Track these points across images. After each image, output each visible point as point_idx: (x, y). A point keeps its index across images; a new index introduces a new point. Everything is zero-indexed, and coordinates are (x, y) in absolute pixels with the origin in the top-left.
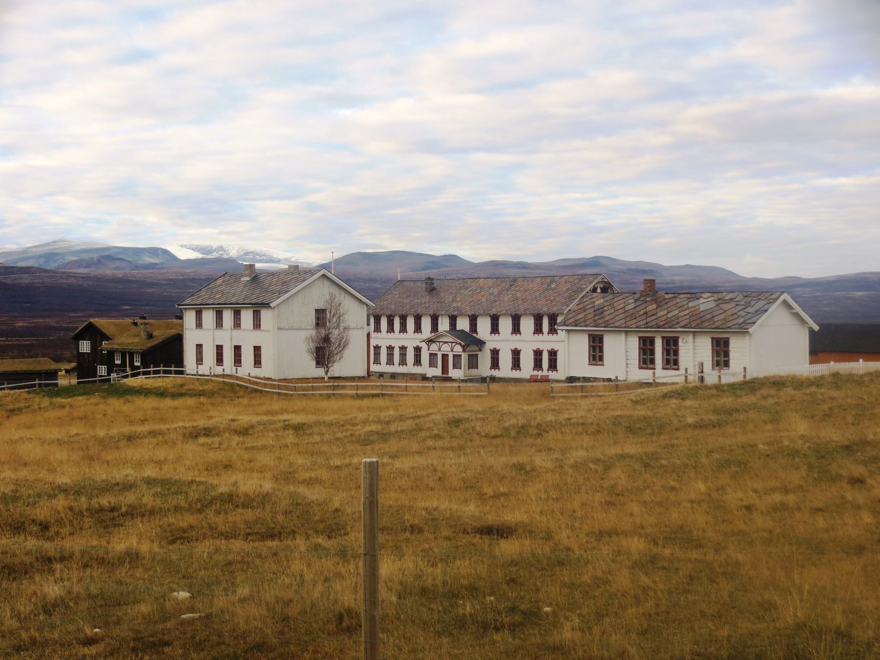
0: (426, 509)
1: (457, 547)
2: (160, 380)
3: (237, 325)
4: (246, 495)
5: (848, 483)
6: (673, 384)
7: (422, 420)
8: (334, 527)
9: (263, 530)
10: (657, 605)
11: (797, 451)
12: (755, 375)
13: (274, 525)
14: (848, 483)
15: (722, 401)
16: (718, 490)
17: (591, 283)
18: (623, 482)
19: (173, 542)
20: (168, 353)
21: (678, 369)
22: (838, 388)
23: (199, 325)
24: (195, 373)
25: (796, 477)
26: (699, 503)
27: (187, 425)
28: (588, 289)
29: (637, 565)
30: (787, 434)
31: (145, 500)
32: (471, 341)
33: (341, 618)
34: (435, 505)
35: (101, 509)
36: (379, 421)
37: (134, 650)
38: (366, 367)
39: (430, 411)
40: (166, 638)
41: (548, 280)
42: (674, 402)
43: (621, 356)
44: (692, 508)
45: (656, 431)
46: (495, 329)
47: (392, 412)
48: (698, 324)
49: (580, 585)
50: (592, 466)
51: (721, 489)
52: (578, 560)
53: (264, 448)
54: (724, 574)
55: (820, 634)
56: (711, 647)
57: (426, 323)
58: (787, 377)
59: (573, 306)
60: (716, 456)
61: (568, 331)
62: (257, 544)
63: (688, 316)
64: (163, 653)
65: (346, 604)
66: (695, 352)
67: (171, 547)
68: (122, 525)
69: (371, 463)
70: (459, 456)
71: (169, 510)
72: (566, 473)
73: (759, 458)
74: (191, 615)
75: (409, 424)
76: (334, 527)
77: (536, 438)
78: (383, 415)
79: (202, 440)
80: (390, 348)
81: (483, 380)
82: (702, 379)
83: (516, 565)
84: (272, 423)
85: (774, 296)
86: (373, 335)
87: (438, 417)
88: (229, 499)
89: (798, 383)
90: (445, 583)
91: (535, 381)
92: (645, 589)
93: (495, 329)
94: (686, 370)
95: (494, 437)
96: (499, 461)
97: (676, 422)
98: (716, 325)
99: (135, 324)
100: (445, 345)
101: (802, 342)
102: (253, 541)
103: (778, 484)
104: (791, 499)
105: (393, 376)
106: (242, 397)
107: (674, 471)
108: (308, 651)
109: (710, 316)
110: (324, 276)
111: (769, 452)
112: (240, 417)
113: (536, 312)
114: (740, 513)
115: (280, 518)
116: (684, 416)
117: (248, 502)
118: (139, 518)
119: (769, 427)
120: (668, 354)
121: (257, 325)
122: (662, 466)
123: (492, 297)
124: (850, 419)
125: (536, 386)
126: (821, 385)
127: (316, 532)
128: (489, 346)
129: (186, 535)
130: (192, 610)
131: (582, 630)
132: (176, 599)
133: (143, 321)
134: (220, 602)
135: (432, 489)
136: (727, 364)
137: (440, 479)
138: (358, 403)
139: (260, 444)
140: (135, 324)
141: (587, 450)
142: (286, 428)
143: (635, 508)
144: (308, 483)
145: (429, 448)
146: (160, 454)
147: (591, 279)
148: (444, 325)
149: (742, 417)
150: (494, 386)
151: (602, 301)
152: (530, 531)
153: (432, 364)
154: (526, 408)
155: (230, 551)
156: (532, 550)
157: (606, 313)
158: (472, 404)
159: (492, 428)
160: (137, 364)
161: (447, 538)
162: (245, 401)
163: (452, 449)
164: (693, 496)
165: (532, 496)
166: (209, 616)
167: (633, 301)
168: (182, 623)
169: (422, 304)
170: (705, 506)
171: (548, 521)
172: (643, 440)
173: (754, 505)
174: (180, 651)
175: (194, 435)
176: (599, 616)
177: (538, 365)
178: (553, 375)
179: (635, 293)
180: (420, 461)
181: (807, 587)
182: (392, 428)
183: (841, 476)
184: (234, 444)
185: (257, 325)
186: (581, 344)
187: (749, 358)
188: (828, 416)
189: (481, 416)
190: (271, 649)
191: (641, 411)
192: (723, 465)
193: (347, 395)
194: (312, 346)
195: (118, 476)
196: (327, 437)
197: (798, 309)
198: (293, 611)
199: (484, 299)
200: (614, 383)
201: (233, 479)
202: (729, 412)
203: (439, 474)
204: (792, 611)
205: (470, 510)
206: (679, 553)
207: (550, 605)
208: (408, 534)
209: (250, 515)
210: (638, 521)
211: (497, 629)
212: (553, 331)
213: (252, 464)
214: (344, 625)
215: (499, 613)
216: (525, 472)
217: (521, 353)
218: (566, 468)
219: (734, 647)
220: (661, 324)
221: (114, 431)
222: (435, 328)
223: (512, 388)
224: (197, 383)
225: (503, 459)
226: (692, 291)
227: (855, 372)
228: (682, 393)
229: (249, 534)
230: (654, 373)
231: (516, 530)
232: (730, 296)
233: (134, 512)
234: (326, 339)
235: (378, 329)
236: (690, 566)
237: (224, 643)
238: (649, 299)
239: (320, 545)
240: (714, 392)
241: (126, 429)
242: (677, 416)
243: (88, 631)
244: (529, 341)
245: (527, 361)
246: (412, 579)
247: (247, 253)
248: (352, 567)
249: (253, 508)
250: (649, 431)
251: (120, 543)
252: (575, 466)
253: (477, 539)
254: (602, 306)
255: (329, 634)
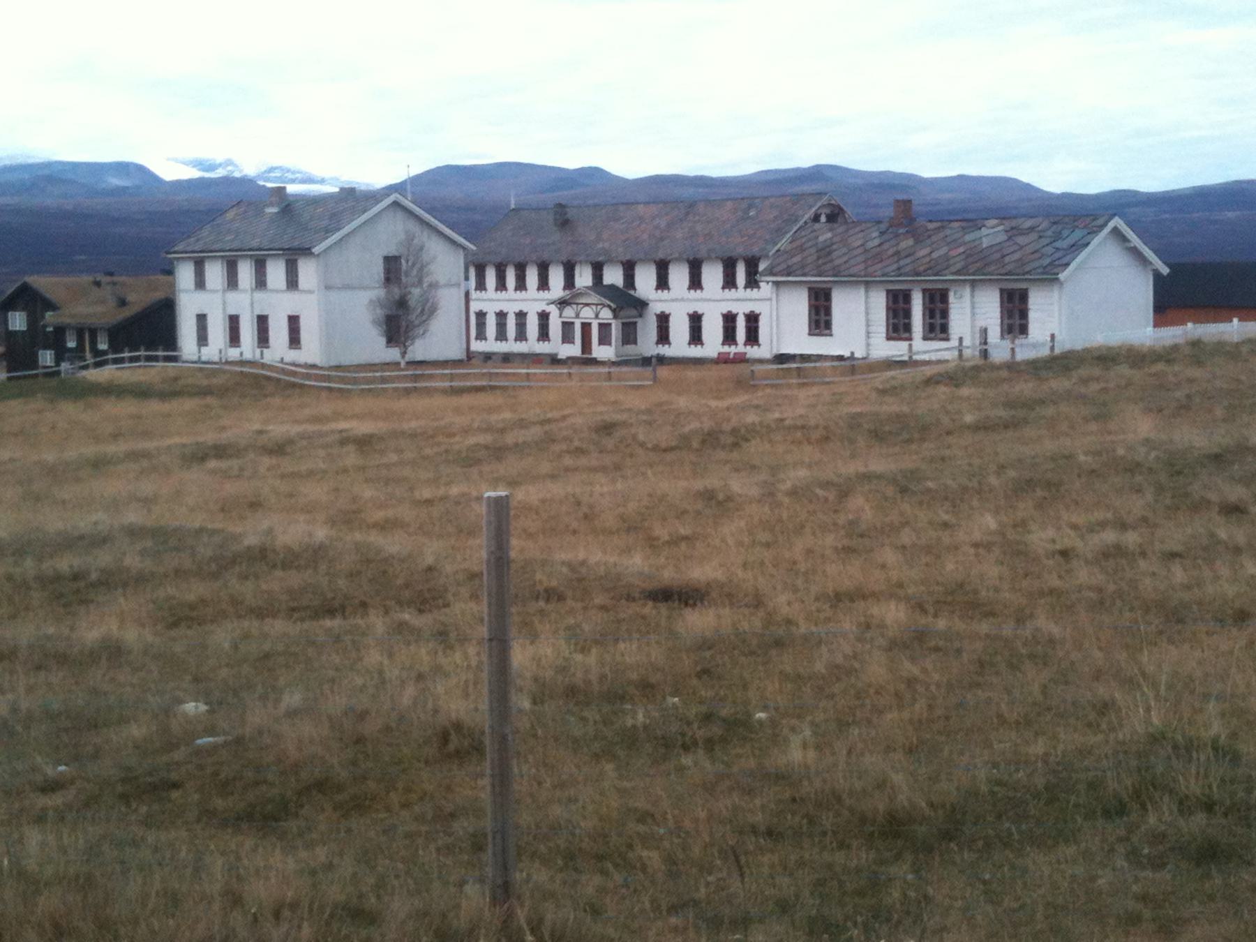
0: (569, 565)
1: (619, 621)
2: (141, 371)
3: (261, 283)
4: (289, 549)
5: (1219, 513)
6: (939, 362)
7: (553, 426)
8: (426, 594)
9: (316, 603)
10: (930, 707)
11: (1138, 465)
12: (1068, 346)
13: (337, 594)
14: (1219, 513)
15: (1017, 388)
16: (1015, 526)
17: (811, 207)
18: (868, 515)
19: (175, 625)
20: (153, 328)
21: (947, 339)
22: (1199, 363)
23: (200, 284)
24: (195, 358)
25: (1136, 506)
26: (988, 546)
27: (185, 440)
28: (807, 217)
29: (893, 645)
30: (1122, 437)
31: (128, 561)
32: (626, 303)
33: (445, 738)
34: (581, 556)
35: (58, 578)
36: (488, 429)
37: (125, 798)
38: (464, 346)
39: (566, 412)
40: (174, 776)
41: (744, 205)
42: (942, 390)
43: (859, 325)
44: (977, 555)
45: (916, 436)
46: (663, 283)
47: (507, 415)
48: (978, 270)
49: (810, 678)
50: (819, 492)
51: (1022, 525)
52: (806, 638)
53: (311, 474)
54: (1032, 656)
55: (1188, 750)
56: (1017, 770)
57: (556, 277)
58: (1120, 347)
59: (783, 243)
60: (1012, 473)
61: (777, 284)
62: (306, 625)
63: (963, 257)
64: (170, 801)
65: (453, 715)
66: (975, 314)
67: (173, 633)
68: (92, 601)
69: (498, 500)
70: (614, 481)
71: (166, 576)
72: (779, 505)
73: (1079, 476)
74: (211, 739)
75: (535, 432)
76: (427, 595)
77: (731, 451)
78: (494, 418)
79: (212, 464)
80: (501, 316)
81: (646, 361)
82: (985, 354)
83: (710, 648)
84: (321, 435)
85: (1100, 221)
86: (474, 295)
87: (579, 420)
88: (262, 556)
89: (1135, 357)
90: (602, 678)
91: (725, 362)
92: (911, 682)
93: (663, 283)
94: (961, 339)
95: (665, 450)
96: (675, 486)
97: (946, 420)
98: (1008, 268)
99: (98, 284)
100: (587, 308)
101: (1142, 293)
102: (302, 620)
103: (1109, 515)
104: (1131, 539)
105: (507, 358)
106: (272, 395)
107: (946, 499)
108: (396, 790)
109: (998, 255)
110: (396, 204)
111: (1094, 466)
112: (271, 428)
113: (729, 254)
114: (1051, 562)
115: (342, 583)
116: (959, 412)
117: (291, 560)
118: (120, 590)
119: (1093, 427)
120: (932, 316)
121: (292, 282)
122: (929, 490)
123: (657, 233)
124: (1219, 412)
125: (727, 371)
126: (1174, 360)
127: (400, 603)
128: (656, 308)
129: (194, 614)
130: (211, 731)
131: (818, 747)
132: (185, 715)
133: (108, 279)
134: (257, 716)
135: (575, 532)
136: (1024, 330)
137: (586, 517)
138: (455, 401)
139: (303, 468)
140: (98, 284)
141: (810, 466)
142: (344, 442)
143: (889, 556)
144: (385, 526)
145: (567, 470)
146: (147, 487)
147: (811, 200)
148: (584, 278)
149: (1050, 411)
150: (663, 372)
151: (829, 235)
152: (728, 594)
153: (567, 338)
154: (714, 403)
155: (265, 636)
156: (734, 625)
157: (835, 255)
158: (633, 399)
159: (664, 436)
160: (103, 346)
161: (603, 608)
162: (277, 401)
163: (603, 469)
164: (977, 536)
165: (730, 541)
166: (239, 741)
167: (875, 234)
168: (199, 752)
169: (549, 245)
170: (997, 551)
171: (756, 578)
172: (897, 449)
173: (1073, 549)
174: (196, 797)
175: (198, 456)
176: (843, 725)
177: (729, 337)
178: (753, 352)
179: (879, 222)
180: (556, 489)
181: (1164, 677)
182: (510, 439)
183: (1209, 502)
184: (262, 470)
185: (292, 282)
186: (797, 305)
187: (1054, 321)
188: (1184, 407)
189: (645, 418)
190: (340, 788)
191: (892, 406)
192: (1023, 487)
193: (436, 390)
194: (380, 313)
195: (82, 524)
196: (409, 455)
197: (1135, 240)
198: (370, 728)
199: (645, 236)
200: (847, 363)
201: (265, 525)
202: (1030, 404)
203: (585, 509)
204: (1142, 716)
205: (637, 563)
206: (960, 625)
207: (765, 708)
208: (542, 604)
209: (295, 579)
210: (894, 575)
211: (686, 748)
212: (752, 283)
213: (293, 501)
214: (451, 747)
215: (689, 723)
216: (717, 503)
217: (704, 319)
218: (780, 496)
219: (1054, 771)
220: (922, 268)
221: (71, 454)
222: (569, 282)
223: (692, 374)
224: (199, 375)
225: (683, 484)
226: (970, 216)
227: (1226, 338)
228: (955, 377)
229: (293, 610)
230: (910, 346)
231: (708, 593)
232: (1028, 224)
233: (110, 581)
234: (402, 303)
235: (481, 286)
236: (979, 645)
237: (265, 782)
238: (901, 231)
239: (406, 623)
240: (1004, 374)
241: (90, 450)
242: (947, 412)
243: (49, 771)
244: (715, 299)
245: (713, 330)
246: (552, 673)
247: (272, 170)
248: (458, 657)
249: (298, 568)
250: (905, 436)
251: (91, 630)
252: (793, 493)
253: (648, 609)
254: (828, 243)
255: (427, 762)
